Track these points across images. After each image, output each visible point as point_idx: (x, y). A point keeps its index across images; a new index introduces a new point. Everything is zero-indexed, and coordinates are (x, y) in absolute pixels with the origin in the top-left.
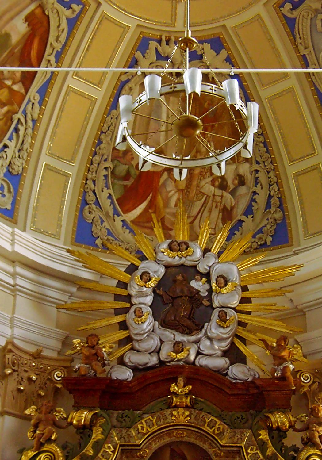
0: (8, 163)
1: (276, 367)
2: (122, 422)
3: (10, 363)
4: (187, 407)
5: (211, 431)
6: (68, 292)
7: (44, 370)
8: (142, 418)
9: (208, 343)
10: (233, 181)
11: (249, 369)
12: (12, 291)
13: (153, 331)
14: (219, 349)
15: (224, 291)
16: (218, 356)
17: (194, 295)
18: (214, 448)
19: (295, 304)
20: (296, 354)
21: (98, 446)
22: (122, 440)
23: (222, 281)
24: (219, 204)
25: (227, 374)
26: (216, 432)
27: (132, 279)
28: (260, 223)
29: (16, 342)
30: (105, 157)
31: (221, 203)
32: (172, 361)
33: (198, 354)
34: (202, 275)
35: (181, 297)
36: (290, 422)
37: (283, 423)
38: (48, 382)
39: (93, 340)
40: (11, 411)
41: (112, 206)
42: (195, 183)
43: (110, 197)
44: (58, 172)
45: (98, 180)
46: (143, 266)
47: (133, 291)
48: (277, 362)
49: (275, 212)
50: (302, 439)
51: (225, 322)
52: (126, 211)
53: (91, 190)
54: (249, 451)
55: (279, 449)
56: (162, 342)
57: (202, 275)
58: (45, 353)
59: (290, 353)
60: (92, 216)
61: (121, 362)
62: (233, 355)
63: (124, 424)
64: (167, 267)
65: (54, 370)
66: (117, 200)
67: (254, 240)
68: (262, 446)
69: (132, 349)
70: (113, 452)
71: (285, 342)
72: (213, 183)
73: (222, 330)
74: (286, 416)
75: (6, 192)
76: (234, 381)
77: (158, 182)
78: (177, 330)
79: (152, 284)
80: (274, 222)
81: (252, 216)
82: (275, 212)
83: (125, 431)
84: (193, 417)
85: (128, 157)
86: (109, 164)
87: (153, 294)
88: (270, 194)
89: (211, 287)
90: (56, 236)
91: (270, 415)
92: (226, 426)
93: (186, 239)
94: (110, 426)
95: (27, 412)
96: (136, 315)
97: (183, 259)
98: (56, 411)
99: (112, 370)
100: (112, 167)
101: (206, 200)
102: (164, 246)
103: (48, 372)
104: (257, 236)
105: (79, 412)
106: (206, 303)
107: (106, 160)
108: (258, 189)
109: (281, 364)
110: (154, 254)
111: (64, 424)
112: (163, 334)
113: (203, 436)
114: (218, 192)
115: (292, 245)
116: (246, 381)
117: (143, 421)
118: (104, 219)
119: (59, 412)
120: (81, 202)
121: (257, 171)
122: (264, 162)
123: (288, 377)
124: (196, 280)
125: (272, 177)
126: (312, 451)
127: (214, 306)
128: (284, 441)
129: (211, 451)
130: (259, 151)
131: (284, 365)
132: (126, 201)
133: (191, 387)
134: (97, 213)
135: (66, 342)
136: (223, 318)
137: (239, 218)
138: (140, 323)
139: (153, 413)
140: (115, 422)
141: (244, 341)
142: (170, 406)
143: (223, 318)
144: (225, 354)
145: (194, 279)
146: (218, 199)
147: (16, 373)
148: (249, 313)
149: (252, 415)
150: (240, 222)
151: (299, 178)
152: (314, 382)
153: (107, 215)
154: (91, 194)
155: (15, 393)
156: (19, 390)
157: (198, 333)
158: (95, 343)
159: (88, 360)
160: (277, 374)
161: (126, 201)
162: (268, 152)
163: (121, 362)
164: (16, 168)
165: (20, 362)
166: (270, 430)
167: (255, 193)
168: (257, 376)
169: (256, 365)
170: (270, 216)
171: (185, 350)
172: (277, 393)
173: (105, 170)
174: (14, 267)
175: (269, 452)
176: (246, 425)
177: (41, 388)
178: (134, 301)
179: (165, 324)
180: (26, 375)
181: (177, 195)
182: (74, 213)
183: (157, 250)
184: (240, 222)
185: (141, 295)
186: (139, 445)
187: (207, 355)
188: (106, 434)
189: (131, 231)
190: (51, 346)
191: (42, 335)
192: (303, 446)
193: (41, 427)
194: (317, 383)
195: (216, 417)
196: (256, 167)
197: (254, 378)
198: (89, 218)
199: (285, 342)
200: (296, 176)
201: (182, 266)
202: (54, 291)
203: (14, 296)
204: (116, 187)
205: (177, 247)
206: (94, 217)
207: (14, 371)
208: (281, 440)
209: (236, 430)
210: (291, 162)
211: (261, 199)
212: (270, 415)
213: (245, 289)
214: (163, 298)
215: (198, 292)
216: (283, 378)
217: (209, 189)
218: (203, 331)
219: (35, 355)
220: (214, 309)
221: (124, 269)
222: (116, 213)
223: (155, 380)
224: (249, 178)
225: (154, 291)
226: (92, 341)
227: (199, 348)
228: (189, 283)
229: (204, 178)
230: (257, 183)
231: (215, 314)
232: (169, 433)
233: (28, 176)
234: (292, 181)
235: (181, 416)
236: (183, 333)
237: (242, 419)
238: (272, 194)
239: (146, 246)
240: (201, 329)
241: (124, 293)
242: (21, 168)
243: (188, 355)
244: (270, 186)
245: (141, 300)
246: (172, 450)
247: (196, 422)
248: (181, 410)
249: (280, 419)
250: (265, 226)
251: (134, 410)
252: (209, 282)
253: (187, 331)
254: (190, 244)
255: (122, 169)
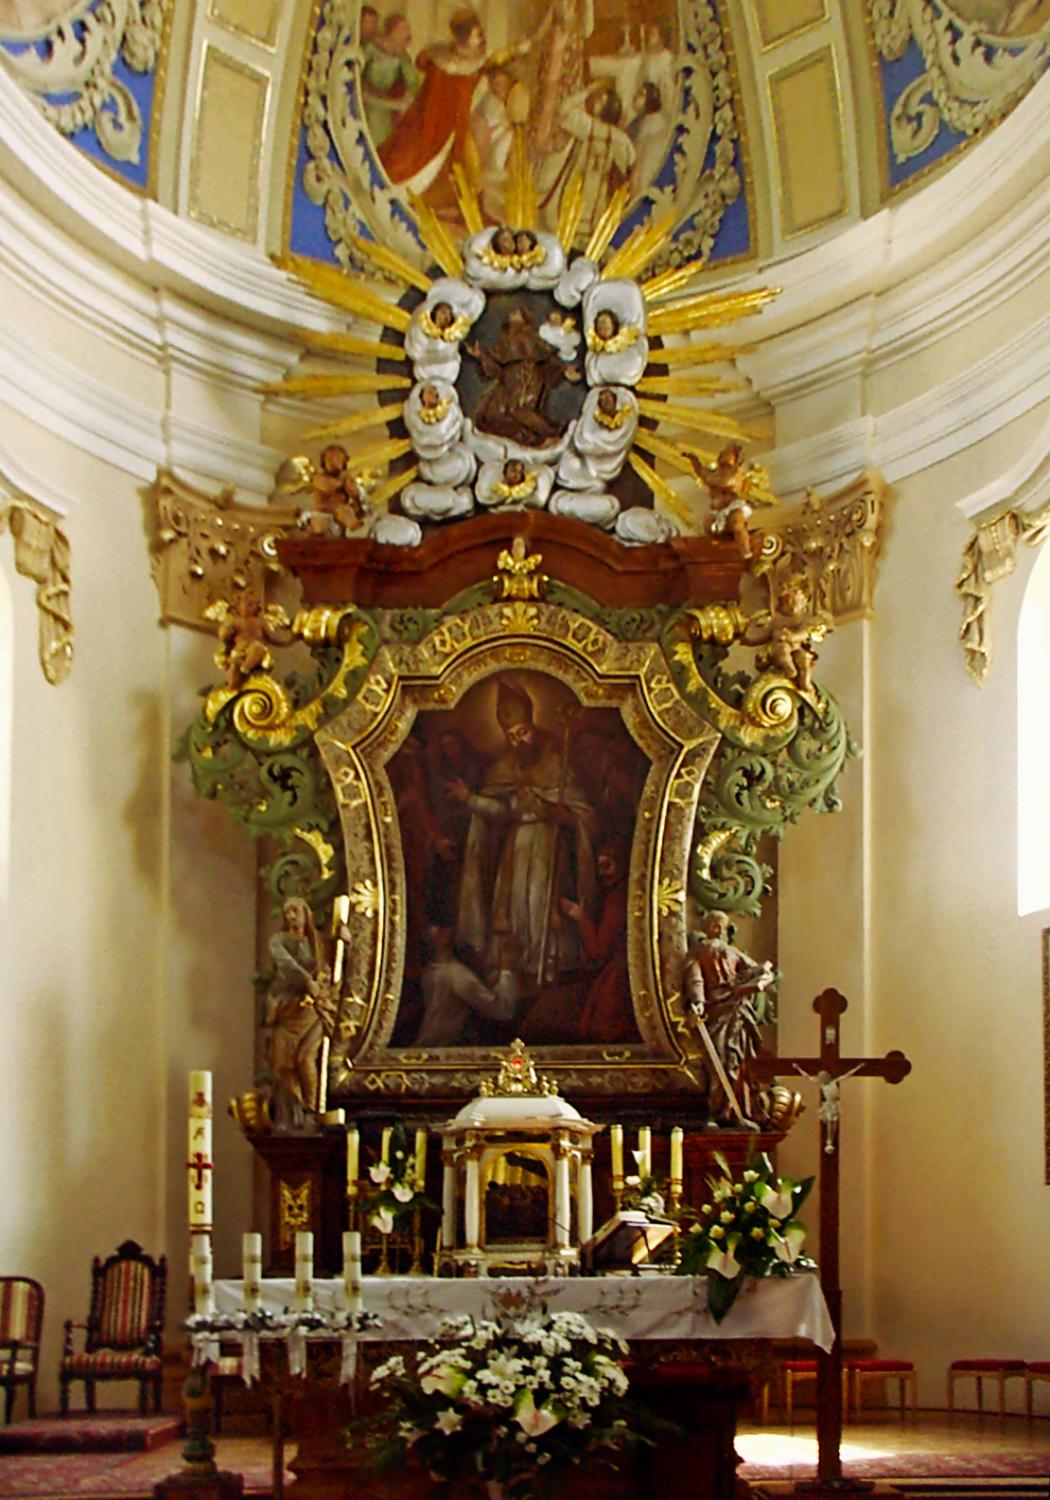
0: (119, 38)
1: (715, 512)
2: (400, 632)
3: (170, 516)
4: (532, 599)
5: (580, 646)
6: (281, 364)
7: (242, 534)
8: (442, 623)
9: (576, 463)
10: (635, 99)
11: (659, 521)
12: (160, 360)
13: (461, 439)
14: (598, 477)
15: (611, 345)
16: (595, 493)
17: (547, 360)
18: (585, 680)
19: (756, 387)
20: (757, 486)
21: (355, 679)
22: (404, 666)
23: (608, 322)
24: (601, 161)
25: (613, 530)
26: (590, 648)
27: (415, 322)
28: (690, 204)
29: (178, 472)
30: (345, 33)
31: (606, 157)
32: (502, 503)
33: (556, 487)
34: (566, 312)
35: (518, 362)
36: (736, 626)
37: (723, 629)
38: (252, 560)
39: (335, 459)
40: (179, 615)
41: (367, 164)
42: (549, 107)
43: (361, 139)
44: (239, 69)
45: (333, 94)
46: (436, 291)
47: (417, 349)
48: (717, 502)
49: (724, 176)
50: (758, 659)
51: (613, 417)
52: (399, 178)
53: (317, 120)
54: (653, 685)
55: (711, 681)
56: (479, 463)
57: (566, 312)
58: (241, 498)
59: (745, 482)
60: (324, 188)
61: (396, 507)
62: (628, 489)
63: (405, 636)
64: (490, 293)
65: (263, 533)
66: (379, 150)
67: (673, 246)
68: (679, 675)
69: (419, 479)
70: (387, 691)
71: (737, 456)
72: (589, 106)
73: (605, 434)
74: (729, 616)
75: (123, 118)
76: (627, 544)
77: (469, 101)
78: (510, 436)
79: (457, 332)
80: (720, 201)
81: (671, 188)
82: (724, 176)
83: (407, 649)
84: (543, 619)
85: (398, 34)
86: (354, 52)
87: (459, 358)
88: (714, 131)
89: (583, 339)
90: (247, 233)
91: (697, 613)
92: (610, 637)
93: (531, 226)
94: (378, 640)
95: (210, 613)
96: (423, 403)
97: (525, 274)
98: (267, 611)
99: (379, 524)
100: (363, 62)
101: (572, 151)
102: (482, 243)
103: (250, 538)
104: (683, 237)
105: (314, 612)
106: (572, 375)
107: (348, 41)
108: (688, 120)
109: (725, 505)
110: (461, 264)
111: (285, 637)
112: (481, 447)
113: (563, 656)
114: (602, 130)
115: (755, 257)
116: (654, 543)
117: (444, 629)
118: (350, 194)
119: (275, 614)
120: (296, 154)
121: (688, 72)
122: (705, 47)
123: (739, 533)
124: (553, 324)
125: (722, 85)
126: (776, 682)
127: (590, 382)
128: (721, 664)
129: (578, 687)
130: (696, 15)
131: (732, 506)
132: (398, 152)
133: (539, 558)
134: (334, 183)
135: (283, 473)
136: (608, 407)
137: (644, 193)
138: (433, 420)
139: (463, 614)
140: (388, 633)
141: (649, 458)
142: (498, 597)
143: (608, 407)
144: (611, 487)
145: (548, 319)
146: (600, 147)
147: (184, 541)
148: (663, 398)
149: (660, 612)
150: (647, 203)
151: (785, 85)
152: (783, 554)
153: (357, 185)
154: (319, 131)
155: (188, 580)
156: (194, 575)
157: (555, 443)
158: (340, 467)
159: (326, 501)
160: (718, 527)
161: (398, 152)
162: (715, 19)
163: (396, 507)
164: (138, 51)
165: (191, 518)
166: (696, 641)
167: (681, 129)
168: (674, 534)
169: (672, 512)
170: (710, 188)
171: (528, 478)
172: (714, 567)
173: (346, 69)
174: (158, 301)
175: (691, 687)
176: (649, 635)
177: (239, 572)
178: (420, 372)
179: (485, 425)
180: (204, 545)
181: (510, 136)
182: (283, 179)
183: (466, 252)
184: (647, 203)
185: (434, 358)
186: (437, 678)
187: (572, 490)
188: (370, 653)
189: (413, 228)
190: (253, 485)
191: (226, 457)
192: (757, 673)
193: (240, 643)
194: (788, 556)
195: (591, 619)
196: (687, 60)
197: (669, 538)
198: (317, 190)
199: (737, 456)
200: (777, 80)
201: (523, 290)
202: (253, 358)
203: (167, 372)
204: (375, 117)
205: (509, 244)
206: (329, 192)
207: (180, 534)
208: (716, 664)
209: (631, 646)
210: (766, 43)
211: (695, 145)
212: (697, 613)
213: (656, 343)
214: (480, 363)
215: (556, 351)
216: (729, 535)
217: (581, 120)
218: (566, 439)
219: (220, 502)
220: (588, 389)
221: (396, 300)
222: (376, 180)
223: (467, 545)
224: (671, 94)
225: (462, 350)
226: (333, 464)
227: (557, 475)
228: (538, 330)
229: (570, 93)
230: (686, 104)
231: (593, 397)
232: (495, 653)
233: (170, 78)
234: (765, 93)
235: (521, 618)
236: (525, 442)
237: (642, 620)
238: (719, 131)
239: (443, 244)
240: (561, 435)
241: (398, 354)
242: (151, 54)
243: (536, 489)
244: (716, 109)
245: (435, 370)
246: (503, 689)
247: (549, 629)
248: (520, 606)
249: (716, 620)
250: (700, 212)
251: (426, 606)
252: (579, 327)
253: (533, 438)
254: (540, 236)
255: (385, 69)
